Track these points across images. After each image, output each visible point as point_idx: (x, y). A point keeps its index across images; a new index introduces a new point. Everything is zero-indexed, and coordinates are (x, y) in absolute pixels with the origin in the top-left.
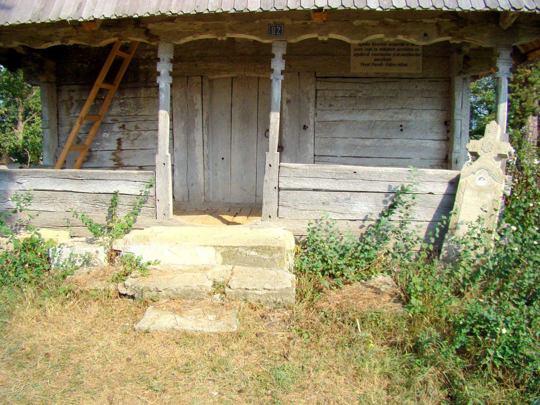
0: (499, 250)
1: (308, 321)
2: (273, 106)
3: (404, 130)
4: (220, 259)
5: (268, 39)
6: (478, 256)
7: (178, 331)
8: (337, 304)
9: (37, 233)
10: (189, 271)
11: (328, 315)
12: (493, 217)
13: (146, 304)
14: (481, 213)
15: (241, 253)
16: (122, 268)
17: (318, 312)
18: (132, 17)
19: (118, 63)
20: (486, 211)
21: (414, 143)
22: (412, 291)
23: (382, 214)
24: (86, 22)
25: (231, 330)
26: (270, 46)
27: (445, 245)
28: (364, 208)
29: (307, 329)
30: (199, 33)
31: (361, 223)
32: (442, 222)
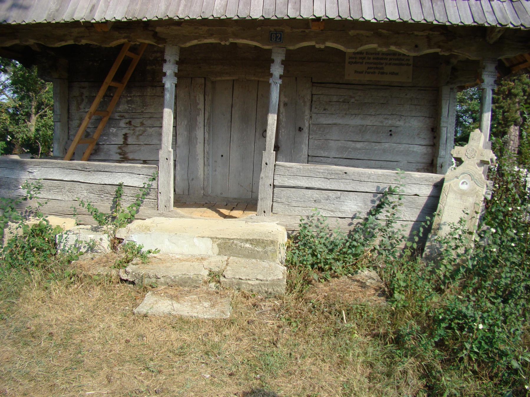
1: (297, 311)
2: (271, 108)
3: (393, 135)
4: (216, 250)
5: (268, 45)
6: (458, 256)
7: (175, 316)
8: (325, 296)
9: (45, 220)
10: (187, 260)
11: (316, 306)
12: (474, 220)
13: (145, 290)
14: (463, 215)
15: (236, 245)
16: (124, 255)
17: (306, 303)
18: (141, 20)
19: (127, 62)
20: (467, 214)
21: (402, 147)
22: (396, 286)
23: (370, 213)
24: (98, 23)
25: (225, 317)
26: (270, 51)
27: (428, 244)
28: (353, 207)
29: (296, 318)
30: (204, 37)
31: (350, 221)
32: (425, 222)
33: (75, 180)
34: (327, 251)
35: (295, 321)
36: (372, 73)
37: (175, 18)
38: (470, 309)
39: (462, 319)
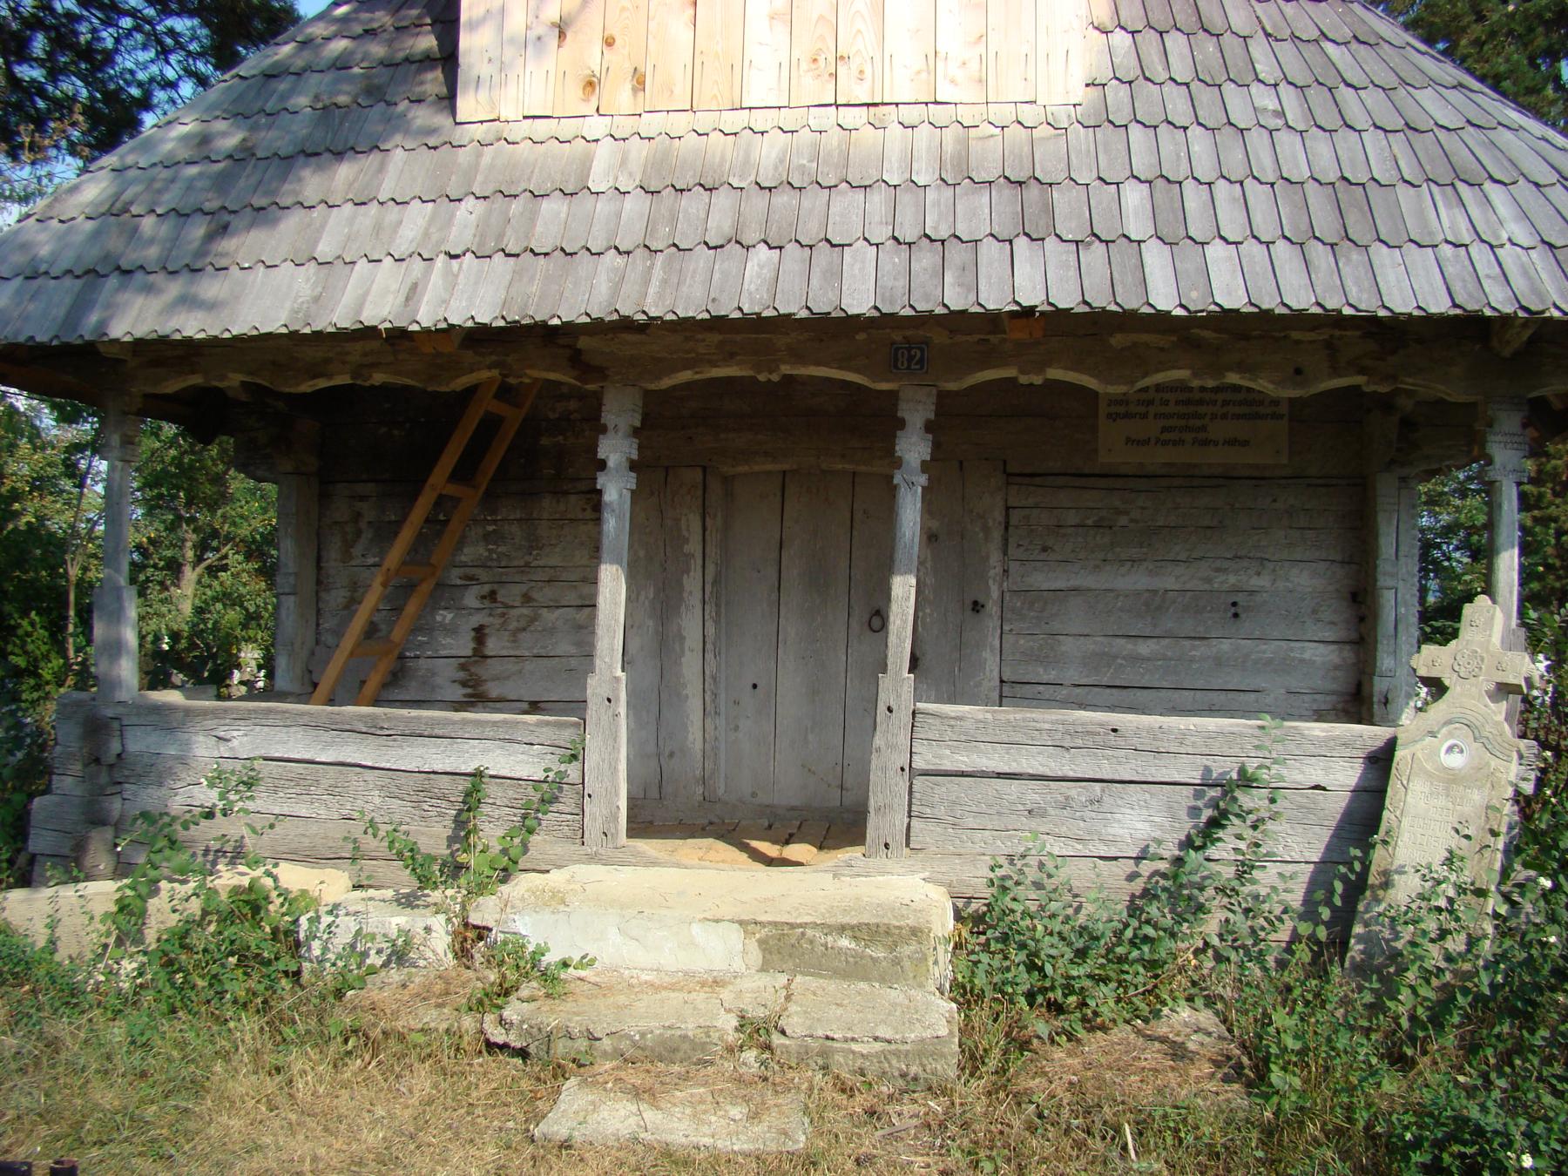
0: (1508, 943)
1: (992, 1128)
2: (900, 555)
3: (1243, 616)
4: (756, 956)
5: (888, 381)
6: (1449, 958)
7: (649, 1147)
8: (1071, 1083)
9: (269, 874)
10: (672, 988)
11: (1046, 1112)
12: (1487, 853)
13: (560, 1072)
14: (1455, 842)
15: (811, 942)
16: (493, 976)
17: (1019, 1104)
18: (545, 322)
19: (490, 426)
20: (1467, 837)
21: (1269, 650)
22: (1274, 1050)
23: (1188, 844)
24: (426, 332)
25: (790, 1146)
26: (893, 396)
27: (1358, 929)
28: (1139, 825)
29: (991, 1149)
31: (1129, 866)
32: (1349, 864)
33: (349, 760)
34: (1069, 954)
35: (989, 1157)
36: (1175, 443)
37: (637, 317)
38: (1494, 1110)
39: (1474, 1143)
